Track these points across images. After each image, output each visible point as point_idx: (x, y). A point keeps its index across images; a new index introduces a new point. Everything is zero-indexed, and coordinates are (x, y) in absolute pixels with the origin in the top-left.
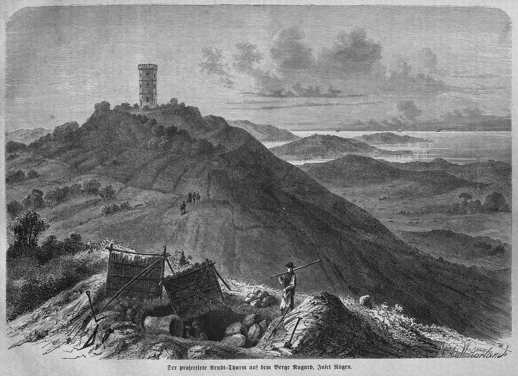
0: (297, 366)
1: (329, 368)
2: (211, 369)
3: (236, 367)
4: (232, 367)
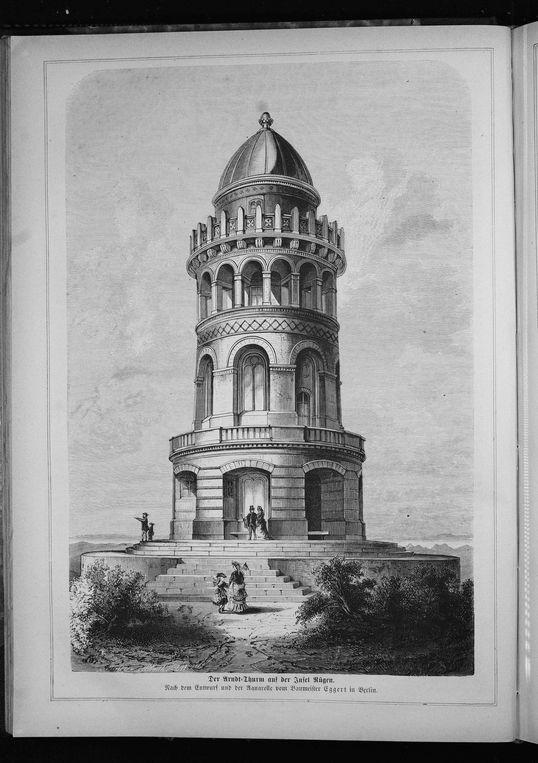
0: (319, 678)
1: (307, 681)
2: (225, 681)
3: (253, 678)
4: (247, 679)
